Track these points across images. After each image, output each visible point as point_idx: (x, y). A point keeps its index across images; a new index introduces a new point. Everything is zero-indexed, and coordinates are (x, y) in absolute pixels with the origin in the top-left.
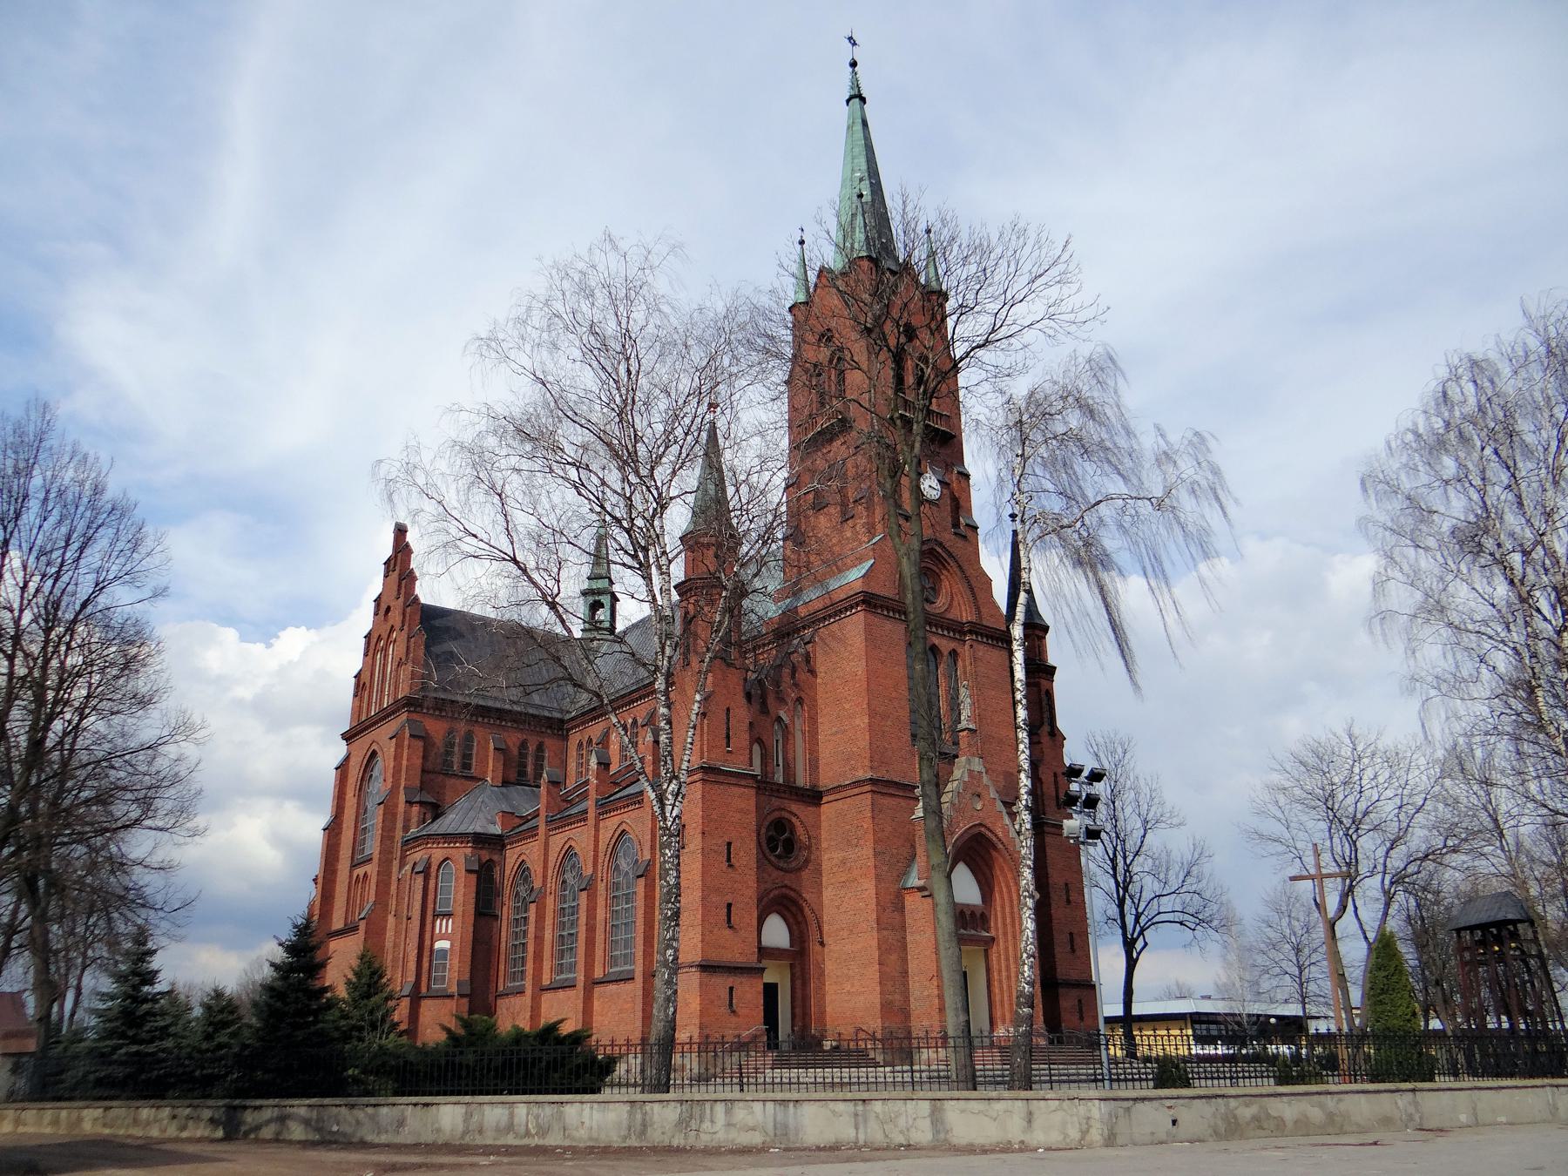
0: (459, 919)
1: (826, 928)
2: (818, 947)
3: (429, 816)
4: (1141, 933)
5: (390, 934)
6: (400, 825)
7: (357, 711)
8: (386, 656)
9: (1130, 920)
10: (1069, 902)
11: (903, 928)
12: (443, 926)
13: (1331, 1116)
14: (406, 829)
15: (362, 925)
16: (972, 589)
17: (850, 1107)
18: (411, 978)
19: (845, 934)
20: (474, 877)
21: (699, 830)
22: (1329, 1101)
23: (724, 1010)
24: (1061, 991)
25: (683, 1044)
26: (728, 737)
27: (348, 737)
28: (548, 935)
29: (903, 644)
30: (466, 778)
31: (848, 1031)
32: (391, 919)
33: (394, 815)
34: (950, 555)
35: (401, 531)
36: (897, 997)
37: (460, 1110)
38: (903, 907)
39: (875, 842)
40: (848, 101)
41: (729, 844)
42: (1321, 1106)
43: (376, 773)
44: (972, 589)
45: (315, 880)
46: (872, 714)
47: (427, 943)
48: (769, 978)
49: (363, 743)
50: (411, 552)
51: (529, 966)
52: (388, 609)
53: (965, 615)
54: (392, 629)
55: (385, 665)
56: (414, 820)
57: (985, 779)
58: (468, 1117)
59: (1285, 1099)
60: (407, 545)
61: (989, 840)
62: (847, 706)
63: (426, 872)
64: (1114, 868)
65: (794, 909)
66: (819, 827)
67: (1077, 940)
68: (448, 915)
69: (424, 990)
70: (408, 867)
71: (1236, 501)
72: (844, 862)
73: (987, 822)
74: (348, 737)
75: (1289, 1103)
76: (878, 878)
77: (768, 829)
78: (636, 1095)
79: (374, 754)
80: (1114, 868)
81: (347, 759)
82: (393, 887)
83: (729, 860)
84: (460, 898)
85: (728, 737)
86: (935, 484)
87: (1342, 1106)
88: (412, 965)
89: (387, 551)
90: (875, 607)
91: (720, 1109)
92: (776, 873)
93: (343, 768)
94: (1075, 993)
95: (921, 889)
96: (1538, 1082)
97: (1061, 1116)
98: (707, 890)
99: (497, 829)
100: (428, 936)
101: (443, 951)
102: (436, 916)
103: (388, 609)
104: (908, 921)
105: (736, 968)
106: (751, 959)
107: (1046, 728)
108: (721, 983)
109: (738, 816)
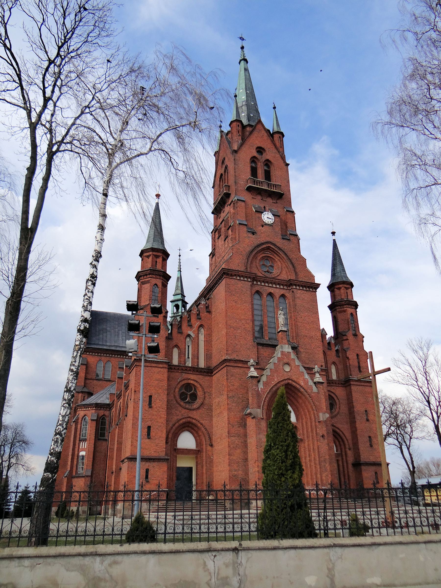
1: (214, 438)
2: (209, 448)
10: (368, 420)
12: (84, 445)
20: (94, 423)
24: (363, 468)
34: (280, 249)
36: (240, 472)
38: (245, 424)
39: (228, 391)
40: (239, 63)
42: (83, 570)
47: (76, 453)
59: (27, 562)
61: (295, 387)
65: (195, 428)
66: (211, 387)
67: (374, 440)
68: (85, 440)
69: (74, 474)
73: (294, 378)
75: (32, 567)
76: (229, 409)
77: (180, 389)
86: (270, 216)
87: (116, 571)
90: (232, 275)
92: (184, 411)
94: (373, 468)
96: (274, 543)
99: (108, 402)
100: (76, 449)
102: (80, 440)
104: (248, 432)
105: (150, 459)
107: (351, 332)
109: (157, 382)
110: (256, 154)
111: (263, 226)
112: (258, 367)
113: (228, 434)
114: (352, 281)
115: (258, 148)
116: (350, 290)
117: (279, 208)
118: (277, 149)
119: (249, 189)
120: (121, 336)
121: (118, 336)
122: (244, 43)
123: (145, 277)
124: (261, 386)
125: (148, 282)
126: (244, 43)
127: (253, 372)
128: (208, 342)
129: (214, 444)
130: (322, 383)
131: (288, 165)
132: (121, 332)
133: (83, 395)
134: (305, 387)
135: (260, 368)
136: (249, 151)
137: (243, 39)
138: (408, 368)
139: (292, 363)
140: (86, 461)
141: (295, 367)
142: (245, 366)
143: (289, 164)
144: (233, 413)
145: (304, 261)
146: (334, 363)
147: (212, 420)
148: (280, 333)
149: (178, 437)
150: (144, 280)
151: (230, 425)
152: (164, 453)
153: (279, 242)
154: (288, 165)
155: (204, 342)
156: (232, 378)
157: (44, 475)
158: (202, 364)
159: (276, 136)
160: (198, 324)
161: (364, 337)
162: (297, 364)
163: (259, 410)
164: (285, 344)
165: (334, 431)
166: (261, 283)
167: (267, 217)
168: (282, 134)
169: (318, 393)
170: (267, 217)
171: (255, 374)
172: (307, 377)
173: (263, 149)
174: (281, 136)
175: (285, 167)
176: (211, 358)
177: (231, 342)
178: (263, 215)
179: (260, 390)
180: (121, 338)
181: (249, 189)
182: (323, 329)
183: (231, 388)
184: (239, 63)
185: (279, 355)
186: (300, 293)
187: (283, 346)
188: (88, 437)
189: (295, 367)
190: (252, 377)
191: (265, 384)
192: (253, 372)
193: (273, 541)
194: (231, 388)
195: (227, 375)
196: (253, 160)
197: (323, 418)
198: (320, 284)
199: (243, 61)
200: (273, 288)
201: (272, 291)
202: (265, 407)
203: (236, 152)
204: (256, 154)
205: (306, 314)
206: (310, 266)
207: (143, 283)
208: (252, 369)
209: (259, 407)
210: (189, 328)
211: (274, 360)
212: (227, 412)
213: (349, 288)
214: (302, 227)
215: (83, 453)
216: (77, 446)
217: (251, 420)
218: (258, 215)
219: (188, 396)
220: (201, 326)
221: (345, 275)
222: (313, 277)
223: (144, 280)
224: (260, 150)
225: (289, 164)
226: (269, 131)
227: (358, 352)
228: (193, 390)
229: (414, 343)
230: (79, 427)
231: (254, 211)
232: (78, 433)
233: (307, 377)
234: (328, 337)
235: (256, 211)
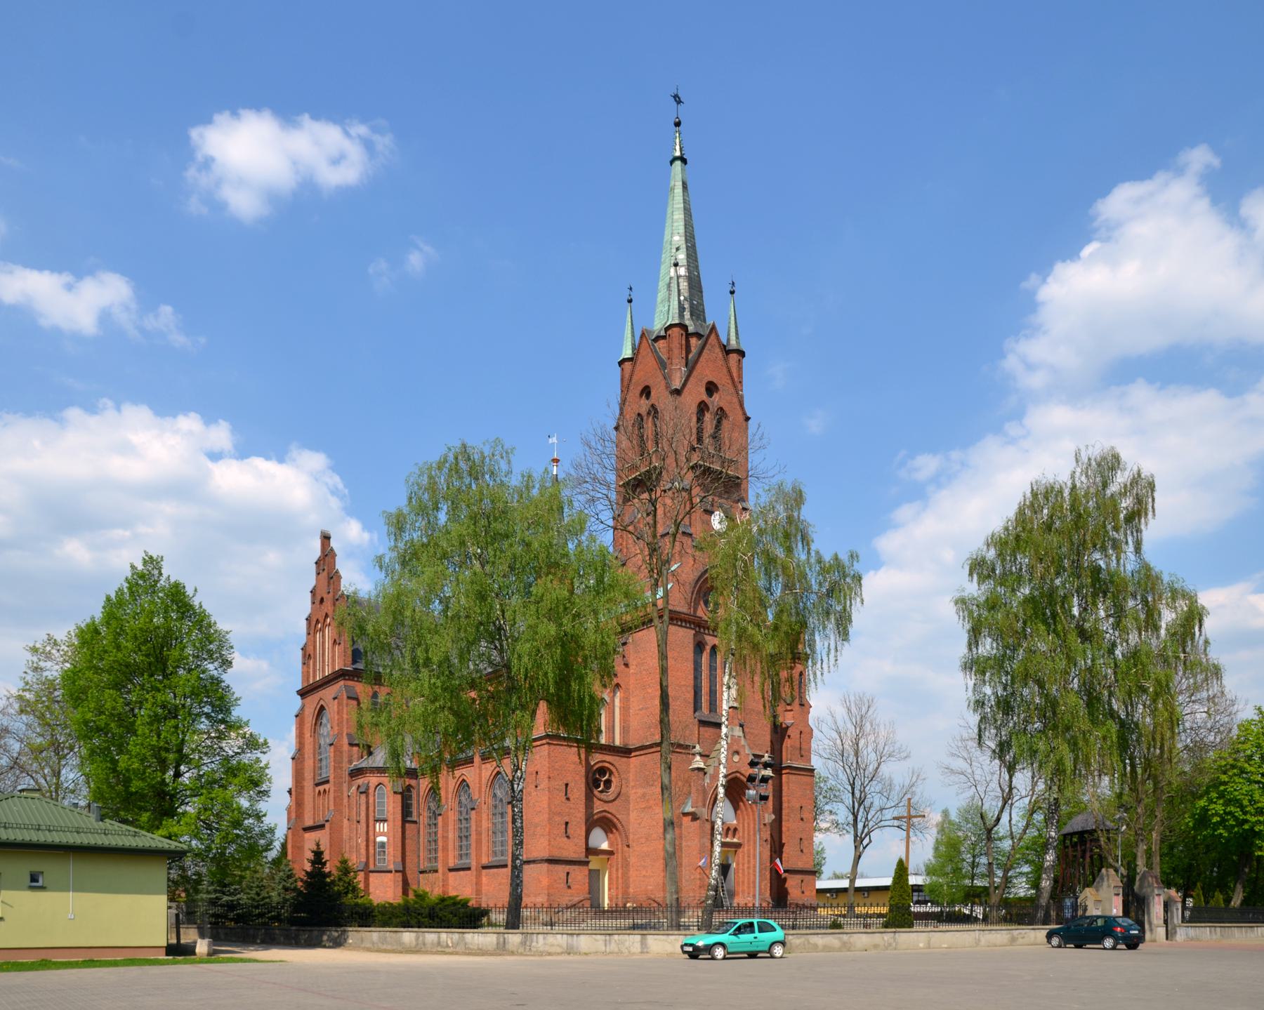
0: (391, 823)
4: (868, 833)
5: (346, 831)
6: (345, 760)
7: (306, 675)
8: (323, 636)
9: (860, 826)
12: (380, 827)
13: (844, 944)
14: (350, 762)
15: (327, 825)
17: (603, 937)
18: (364, 860)
19: (643, 840)
20: (399, 797)
22: (845, 937)
23: (563, 885)
27: (303, 693)
28: (451, 835)
29: (691, 646)
31: (642, 898)
32: (345, 821)
35: (326, 538)
37: (413, 935)
43: (324, 721)
45: (290, 792)
47: (371, 838)
48: (591, 866)
49: (313, 700)
50: (340, 577)
51: (440, 854)
52: (322, 600)
54: (327, 616)
55: (324, 643)
57: (743, 742)
58: (417, 939)
60: (332, 550)
63: (366, 792)
64: (853, 789)
68: (385, 821)
70: (354, 788)
71: (862, 601)
72: (644, 795)
74: (303, 693)
78: (502, 930)
79: (322, 708)
80: (853, 789)
81: (302, 709)
82: (345, 800)
84: (391, 808)
88: (363, 851)
89: (317, 553)
91: (541, 937)
97: (812, 949)
100: (371, 833)
101: (382, 845)
103: (322, 600)
106: (582, 857)
107: (797, 701)
108: (561, 870)
110: (704, 397)
118: (735, 386)
127: (698, 762)
128: (625, 709)
131: (748, 419)
136: (695, 393)
138: (835, 735)
139: (741, 751)
154: (748, 419)
157: (985, 919)
158: (617, 743)
168: (742, 354)
171: (702, 765)
184: (672, 162)
188: (391, 818)
203: (678, 392)
208: (698, 758)
209: (704, 805)
215: (380, 839)
216: (371, 828)
218: (706, 516)
224: (711, 388)
229: (852, 698)
230: (371, 801)
232: (371, 809)
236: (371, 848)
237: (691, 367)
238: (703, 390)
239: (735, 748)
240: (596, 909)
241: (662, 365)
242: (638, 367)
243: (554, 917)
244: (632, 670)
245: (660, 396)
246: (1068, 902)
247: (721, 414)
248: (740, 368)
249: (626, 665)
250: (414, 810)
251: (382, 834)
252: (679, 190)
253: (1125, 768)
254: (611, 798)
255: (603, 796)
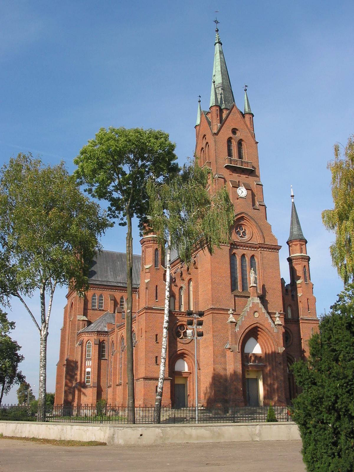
3: (86, 325)
11: (225, 363)
16: (261, 231)
21: (145, 331)
25: (83, 407)
26: (156, 296)
30: (100, 310)
33: (75, 325)
39: (213, 332)
41: (157, 335)
44: (261, 231)
46: (213, 283)
47: (83, 369)
53: (257, 240)
56: (81, 326)
62: (206, 281)
68: (89, 359)
73: (261, 322)
76: (214, 345)
83: (156, 340)
85: (156, 296)
93: (66, 308)
95: (230, 349)
98: (147, 352)
100: (83, 367)
101: (88, 373)
110: (231, 135)
111: (238, 199)
112: (235, 313)
113: (214, 362)
114: (306, 239)
115: (233, 129)
116: (304, 246)
117: (251, 180)
119: (227, 167)
120: (109, 271)
121: (107, 272)
122: (219, 26)
123: (148, 242)
124: (237, 329)
125: (151, 247)
126: (219, 26)
127: (232, 318)
129: (201, 368)
130: (281, 325)
132: (109, 268)
133: (84, 323)
134: (269, 328)
135: (236, 314)
136: (226, 133)
137: (218, 23)
140: (92, 376)
141: (262, 314)
142: (226, 313)
143: (258, 142)
144: (216, 348)
145: (270, 227)
146: (290, 305)
147: (199, 351)
148: (252, 288)
149: (175, 363)
150: (147, 245)
151: (215, 356)
152: (168, 375)
153: (250, 211)
154: (257, 143)
155: (193, 292)
156: (216, 322)
159: (247, 117)
160: (188, 278)
161: (313, 285)
162: (263, 312)
163: (236, 346)
164: (255, 297)
165: (288, 357)
166: (237, 247)
167: (242, 192)
169: (278, 332)
170: (242, 192)
172: (271, 322)
173: (237, 130)
174: (251, 116)
175: (255, 145)
176: (198, 304)
177: (215, 295)
178: (238, 190)
179: (237, 331)
180: (109, 274)
181: (227, 167)
182: (283, 278)
183: (215, 329)
184: (215, 45)
185: (251, 306)
186: (267, 254)
187: (254, 298)
189: (262, 314)
190: (231, 322)
191: (240, 328)
192: (232, 318)
193: (48, 438)
194: (215, 329)
195: (212, 320)
196: (229, 140)
197: (281, 351)
198: (281, 246)
199: (218, 44)
200: (246, 250)
201: (245, 253)
202: (240, 344)
204: (231, 135)
205: (271, 270)
206: (274, 232)
207: (147, 247)
208: (231, 316)
209: (236, 344)
210: (182, 281)
211: (247, 309)
212: (212, 347)
213: (304, 244)
214: (269, 198)
215: (88, 370)
217: (230, 352)
219: (182, 333)
220: (190, 280)
221: (301, 233)
222: (276, 240)
223: (147, 245)
224: (234, 131)
225: (258, 142)
226: (241, 112)
227: (309, 297)
228: (186, 329)
230: (84, 350)
231: (232, 186)
233: (271, 322)
234: (286, 284)
235: (233, 187)
236: (83, 375)
237: (222, 122)
238: (231, 132)
239: (255, 309)
240: (159, 422)
241: (209, 123)
242: (201, 127)
243: (145, 421)
244: (199, 270)
245: (210, 139)
246: (109, 181)
247: (240, 143)
248: (292, 228)
249: (197, 268)
250: (106, 354)
251: (89, 367)
252: (218, 55)
253: (76, 351)
254: (188, 342)
255: (183, 341)
